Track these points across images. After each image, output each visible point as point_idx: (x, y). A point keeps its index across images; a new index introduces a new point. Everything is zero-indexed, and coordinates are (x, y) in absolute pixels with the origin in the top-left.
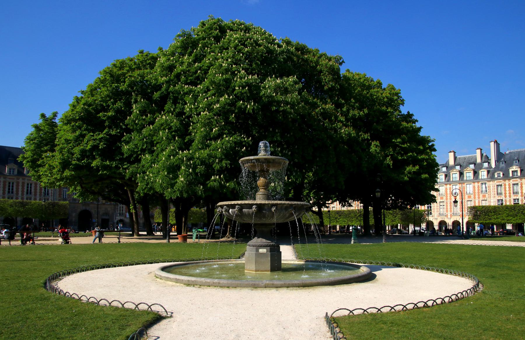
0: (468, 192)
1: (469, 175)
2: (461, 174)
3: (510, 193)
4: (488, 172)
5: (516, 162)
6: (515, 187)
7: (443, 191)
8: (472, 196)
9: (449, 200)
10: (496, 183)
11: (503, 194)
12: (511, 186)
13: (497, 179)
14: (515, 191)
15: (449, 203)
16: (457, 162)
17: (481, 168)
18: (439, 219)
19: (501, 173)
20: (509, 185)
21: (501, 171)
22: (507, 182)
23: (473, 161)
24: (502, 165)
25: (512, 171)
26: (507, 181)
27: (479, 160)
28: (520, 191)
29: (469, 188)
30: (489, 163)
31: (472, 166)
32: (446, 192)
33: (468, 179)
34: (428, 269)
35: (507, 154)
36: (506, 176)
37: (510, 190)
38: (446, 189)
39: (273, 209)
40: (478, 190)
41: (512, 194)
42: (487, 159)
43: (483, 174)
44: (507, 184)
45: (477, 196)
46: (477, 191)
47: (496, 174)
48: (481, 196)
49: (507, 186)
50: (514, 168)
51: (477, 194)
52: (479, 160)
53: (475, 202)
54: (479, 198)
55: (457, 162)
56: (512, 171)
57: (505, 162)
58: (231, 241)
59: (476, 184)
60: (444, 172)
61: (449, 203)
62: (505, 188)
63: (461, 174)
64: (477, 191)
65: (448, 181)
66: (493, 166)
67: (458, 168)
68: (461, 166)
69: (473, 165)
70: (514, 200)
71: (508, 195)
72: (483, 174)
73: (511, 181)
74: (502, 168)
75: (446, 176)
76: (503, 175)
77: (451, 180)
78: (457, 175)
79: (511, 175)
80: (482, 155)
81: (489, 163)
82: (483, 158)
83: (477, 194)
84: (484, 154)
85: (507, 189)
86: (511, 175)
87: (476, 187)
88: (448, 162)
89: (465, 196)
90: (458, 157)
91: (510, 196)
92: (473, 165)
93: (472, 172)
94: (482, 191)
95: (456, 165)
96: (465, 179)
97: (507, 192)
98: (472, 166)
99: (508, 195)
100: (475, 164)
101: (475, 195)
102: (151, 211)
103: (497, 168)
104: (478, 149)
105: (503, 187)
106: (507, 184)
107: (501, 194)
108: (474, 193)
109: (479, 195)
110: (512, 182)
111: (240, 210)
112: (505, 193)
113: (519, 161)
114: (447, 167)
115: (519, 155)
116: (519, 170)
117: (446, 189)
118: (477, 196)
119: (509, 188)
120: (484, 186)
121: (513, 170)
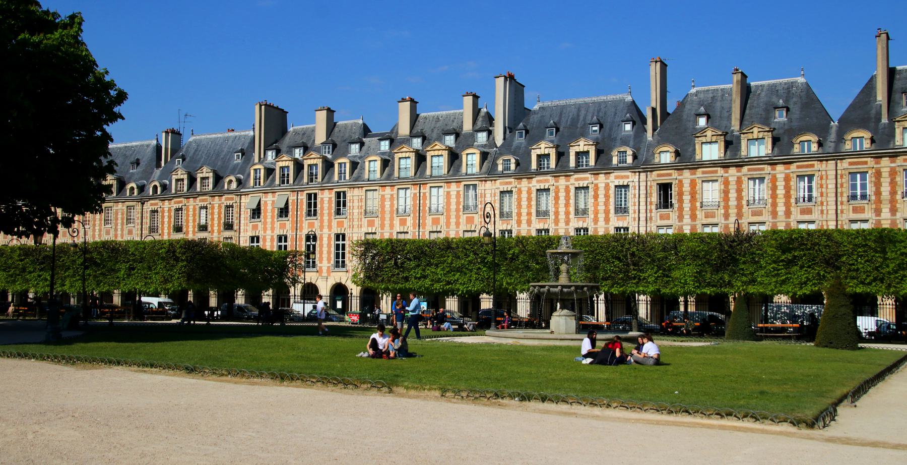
0: (434, 207)
1: (438, 162)
2: (421, 159)
3: (529, 214)
4: (484, 156)
5: (551, 134)
7: (91, 215)
8: (443, 219)
11: (552, 217)
12: (534, 195)
13: (503, 175)
14: (582, 206)
16: (418, 128)
17: (471, 146)
18: (332, 282)
20: (529, 192)
21: (514, 154)
22: (562, 181)
23: (455, 125)
24: (519, 140)
25: (539, 156)
26: (687, 173)
27: (468, 126)
28: (552, 209)
29: (437, 197)
30: (490, 133)
31: (450, 140)
32: (383, 206)
33: (435, 173)
34: (190, 370)
35: (535, 112)
36: (523, 171)
37: (529, 206)
38: (383, 198)
40: (458, 203)
41: (572, 216)
43: (471, 160)
44: (780, 177)
45: (453, 220)
46: (453, 207)
47: (500, 162)
48: (463, 218)
49: (524, 195)
50: (582, 145)
51: (453, 214)
52: (468, 126)
55: (418, 128)
56: (539, 156)
57: (527, 132)
59: (454, 186)
62: (519, 200)
63: (421, 159)
64: (453, 207)
65: (390, 176)
69: (452, 137)
71: (524, 218)
72: (471, 160)
73: (793, 167)
74: (518, 147)
76: (518, 164)
77: (396, 174)
80: (476, 112)
82: (480, 119)
83: (453, 214)
84: (484, 110)
85: (524, 203)
86: (534, 166)
88: (461, 127)
89: (425, 219)
90: (422, 115)
91: (607, 220)
92: (452, 137)
94: (466, 208)
95: (413, 135)
96: (428, 172)
97: (524, 211)
98: (450, 140)
99: (524, 218)
100: (457, 135)
103: (507, 147)
104: (468, 95)
106: (780, 177)
107: (546, 213)
108: (448, 210)
109: (458, 217)
110: (536, 183)
113: (558, 130)
115: (561, 114)
116: (553, 153)
117: (383, 198)
118: (453, 220)
119: (529, 199)
120: (471, 192)
121: (539, 152)
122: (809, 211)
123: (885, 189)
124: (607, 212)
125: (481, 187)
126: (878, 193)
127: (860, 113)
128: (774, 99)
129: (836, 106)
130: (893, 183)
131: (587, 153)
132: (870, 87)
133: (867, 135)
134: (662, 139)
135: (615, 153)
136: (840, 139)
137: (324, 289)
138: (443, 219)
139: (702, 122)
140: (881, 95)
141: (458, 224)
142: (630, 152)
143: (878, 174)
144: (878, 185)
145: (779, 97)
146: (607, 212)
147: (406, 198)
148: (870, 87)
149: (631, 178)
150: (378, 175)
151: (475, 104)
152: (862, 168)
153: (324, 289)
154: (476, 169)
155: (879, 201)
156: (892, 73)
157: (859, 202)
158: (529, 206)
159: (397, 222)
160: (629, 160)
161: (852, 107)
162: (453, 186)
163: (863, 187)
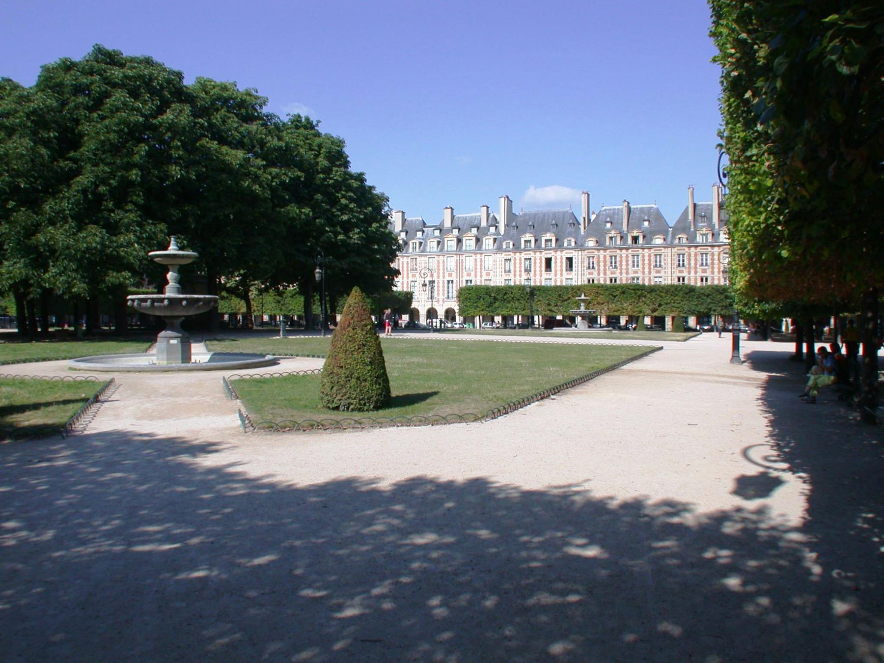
1: (469, 243)
2: (459, 241)
6: (507, 264)
9: (441, 278)
10: (504, 256)
15: (441, 282)
17: (486, 235)
19: (511, 243)
21: (511, 239)
22: (538, 254)
23: (476, 223)
26: (518, 254)
27: (484, 224)
28: (512, 269)
29: (469, 262)
30: (496, 227)
33: (468, 249)
36: (517, 248)
39: (184, 303)
42: (495, 223)
44: (646, 255)
47: (504, 243)
49: (518, 261)
50: (548, 236)
51: (479, 270)
52: (484, 224)
53: (556, 281)
54: (481, 276)
55: (455, 224)
58: (22, 409)
60: (436, 237)
61: (441, 282)
62: (515, 264)
63: (459, 241)
66: (502, 230)
67: (456, 232)
68: (459, 229)
70: (467, 281)
71: (518, 273)
72: (488, 243)
73: (652, 250)
75: (439, 243)
78: (473, 242)
79: (523, 246)
81: (496, 227)
82: (490, 220)
83: (479, 270)
85: (518, 265)
87: (441, 261)
88: (442, 223)
91: (562, 275)
93: (474, 239)
96: (464, 248)
97: (518, 270)
98: (474, 230)
99: (518, 273)
100: (478, 228)
101: (476, 273)
102: (747, 568)
103: (507, 236)
105: (512, 261)
106: (646, 255)
107: (509, 271)
108: (476, 269)
109: (481, 272)
110: (524, 255)
111: (153, 303)
112: (515, 271)
114: (441, 231)
116: (533, 240)
122: (659, 272)
123: (692, 262)
124: (561, 271)
125: (419, 259)
126: (689, 264)
127: (682, 226)
128: (643, 215)
129: (672, 219)
130: (696, 260)
131: (551, 240)
132: (686, 211)
133: (685, 236)
134: (588, 235)
135: (566, 240)
136: (673, 237)
137: (441, 313)
138: (473, 274)
139: (608, 225)
140: (691, 217)
141: (481, 276)
142: (573, 240)
143: (690, 255)
144: (689, 260)
145: (645, 215)
146: (561, 271)
147: (452, 262)
148: (686, 211)
149: (574, 254)
150: (435, 249)
151: (452, 213)
152: (683, 252)
153: (441, 313)
154: (491, 247)
155: (690, 268)
156: (695, 205)
157: (681, 268)
158: (520, 267)
159: (446, 274)
160: (573, 244)
161: (679, 222)
162: (478, 256)
163: (706, 260)
